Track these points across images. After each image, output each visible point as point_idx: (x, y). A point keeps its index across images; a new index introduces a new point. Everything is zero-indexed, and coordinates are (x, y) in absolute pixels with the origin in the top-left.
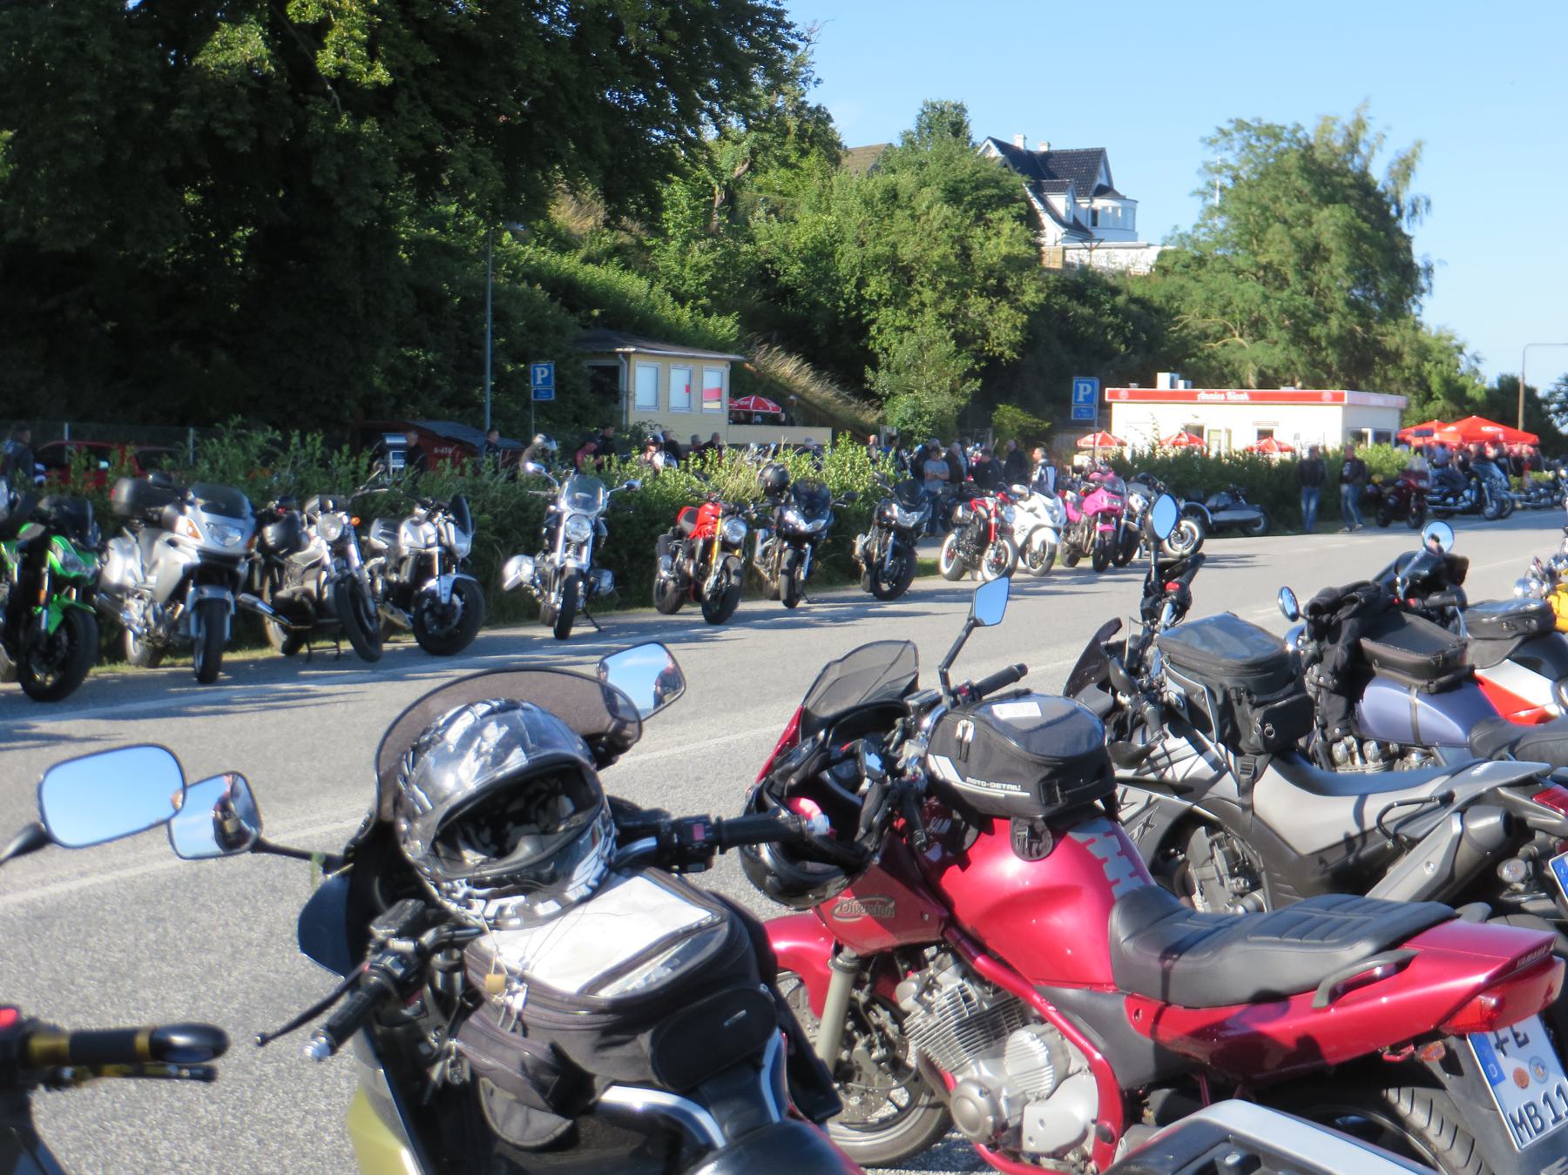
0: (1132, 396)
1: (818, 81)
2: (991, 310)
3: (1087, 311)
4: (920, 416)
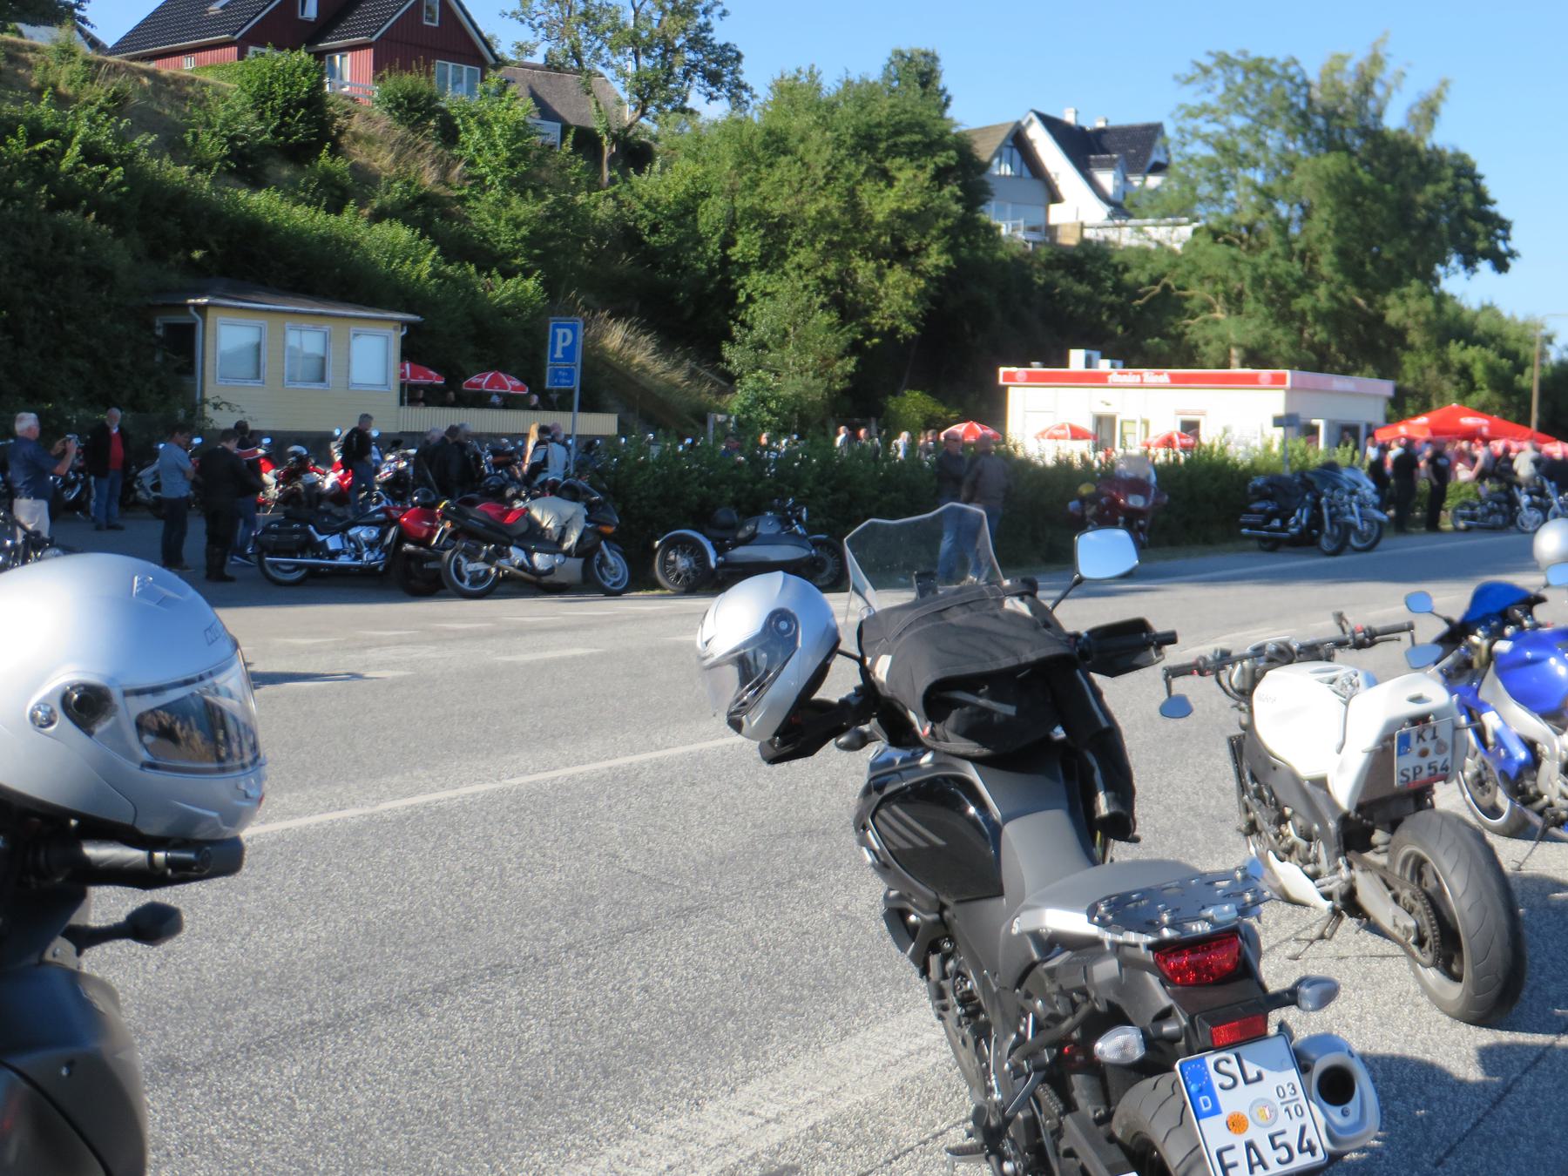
0: (1032, 378)
1: (724, 13)
2: (880, 276)
3: (1083, 289)
4: (764, 400)
